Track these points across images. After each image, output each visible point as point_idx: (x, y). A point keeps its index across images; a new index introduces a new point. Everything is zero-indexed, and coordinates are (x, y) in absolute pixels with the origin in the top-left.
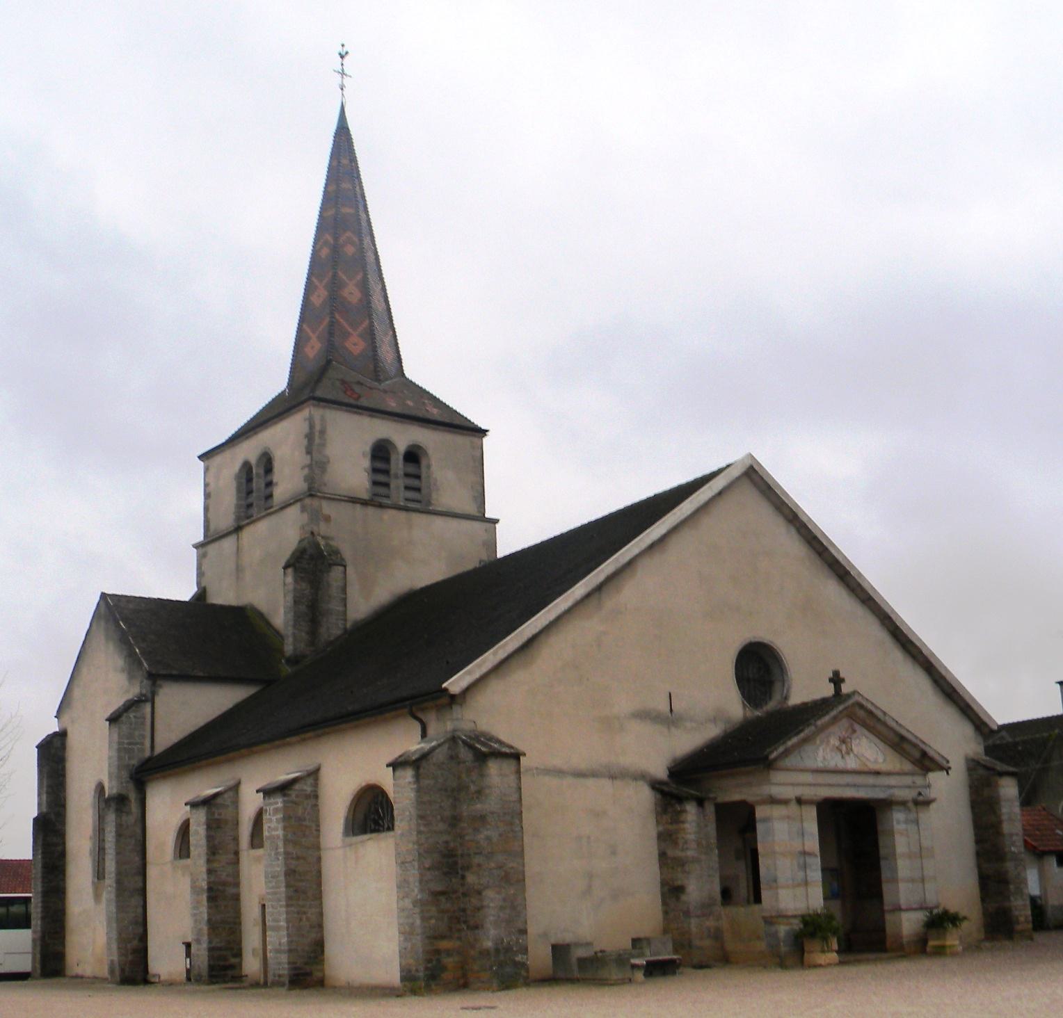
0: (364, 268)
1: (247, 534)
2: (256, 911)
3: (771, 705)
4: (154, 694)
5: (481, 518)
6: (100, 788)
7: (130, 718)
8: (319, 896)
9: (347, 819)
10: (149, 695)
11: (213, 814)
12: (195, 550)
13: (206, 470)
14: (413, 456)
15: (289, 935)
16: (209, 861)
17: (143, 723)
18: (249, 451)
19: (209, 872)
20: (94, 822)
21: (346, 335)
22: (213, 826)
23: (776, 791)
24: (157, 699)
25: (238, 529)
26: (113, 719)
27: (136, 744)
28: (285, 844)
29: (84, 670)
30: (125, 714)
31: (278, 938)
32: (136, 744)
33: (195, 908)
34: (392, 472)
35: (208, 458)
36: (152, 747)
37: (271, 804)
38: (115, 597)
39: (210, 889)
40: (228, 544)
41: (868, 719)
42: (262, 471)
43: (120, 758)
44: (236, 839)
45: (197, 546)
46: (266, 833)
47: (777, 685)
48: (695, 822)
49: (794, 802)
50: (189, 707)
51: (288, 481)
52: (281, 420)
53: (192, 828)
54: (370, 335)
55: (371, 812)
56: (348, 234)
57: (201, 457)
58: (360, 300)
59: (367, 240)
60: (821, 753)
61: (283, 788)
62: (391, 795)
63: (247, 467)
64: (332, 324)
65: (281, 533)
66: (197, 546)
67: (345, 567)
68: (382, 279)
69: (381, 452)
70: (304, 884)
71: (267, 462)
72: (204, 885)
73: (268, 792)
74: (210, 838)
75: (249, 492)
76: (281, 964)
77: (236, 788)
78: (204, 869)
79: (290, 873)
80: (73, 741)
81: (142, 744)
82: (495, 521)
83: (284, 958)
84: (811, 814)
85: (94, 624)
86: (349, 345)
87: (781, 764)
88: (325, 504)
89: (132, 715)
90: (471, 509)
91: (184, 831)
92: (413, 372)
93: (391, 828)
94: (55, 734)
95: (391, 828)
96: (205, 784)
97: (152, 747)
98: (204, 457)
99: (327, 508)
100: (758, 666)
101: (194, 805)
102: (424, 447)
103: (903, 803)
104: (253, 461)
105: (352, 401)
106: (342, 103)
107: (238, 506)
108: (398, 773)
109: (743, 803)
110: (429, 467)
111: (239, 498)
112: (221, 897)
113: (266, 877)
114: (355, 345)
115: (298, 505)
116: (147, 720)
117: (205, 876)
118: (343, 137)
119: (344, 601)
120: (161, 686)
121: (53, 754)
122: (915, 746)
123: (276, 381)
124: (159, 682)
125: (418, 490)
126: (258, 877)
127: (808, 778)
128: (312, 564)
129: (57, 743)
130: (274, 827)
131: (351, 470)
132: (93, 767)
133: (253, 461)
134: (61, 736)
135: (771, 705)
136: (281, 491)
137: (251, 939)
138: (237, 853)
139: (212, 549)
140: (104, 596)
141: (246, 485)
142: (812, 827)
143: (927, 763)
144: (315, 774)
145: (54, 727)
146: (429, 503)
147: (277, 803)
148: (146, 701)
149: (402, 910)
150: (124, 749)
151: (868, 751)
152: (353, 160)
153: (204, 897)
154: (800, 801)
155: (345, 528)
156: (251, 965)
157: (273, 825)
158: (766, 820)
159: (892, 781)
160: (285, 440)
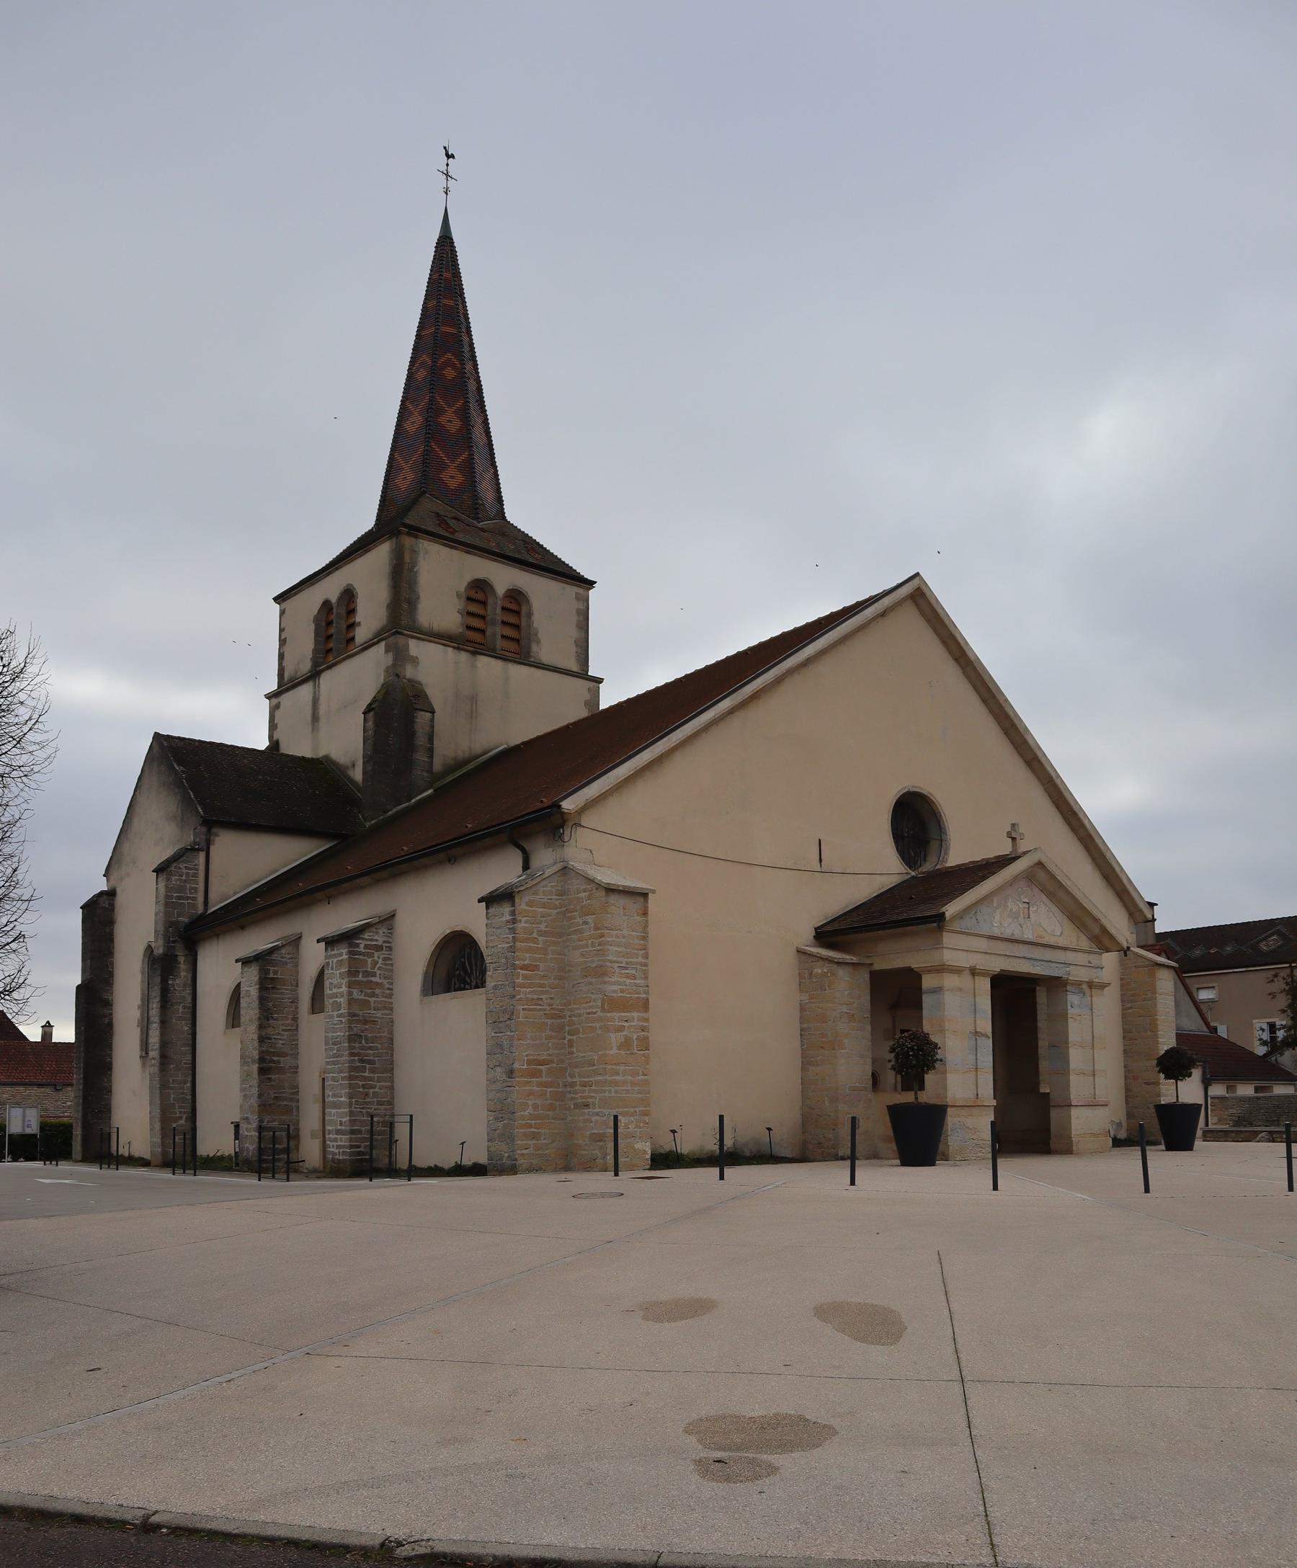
0: (464, 392)
1: (326, 679)
2: (316, 1088)
3: (927, 867)
5: (583, 674)
6: (149, 949)
8: (389, 1068)
9: (426, 974)
10: (203, 844)
11: (267, 972)
13: (282, 613)
14: (516, 597)
15: (351, 1113)
16: (261, 1027)
17: (195, 875)
18: (330, 589)
19: (262, 1040)
20: (245, 1078)
21: (443, 466)
22: (267, 985)
23: (949, 957)
24: (214, 850)
25: (314, 675)
26: (159, 870)
27: (188, 898)
28: (349, 1004)
29: (136, 821)
31: (339, 1117)
32: (188, 898)
33: (243, 1081)
36: (206, 903)
37: (335, 956)
38: (169, 738)
39: (262, 1060)
40: (305, 691)
41: (1044, 881)
42: (343, 612)
43: (167, 914)
44: (295, 1001)
45: (269, 696)
46: (327, 992)
47: (934, 845)
48: (847, 991)
49: (967, 972)
50: (244, 861)
51: (370, 615)
52: (367, 551)
53: (244, 988)
54: (468, 467)
55: (458, 965)
56: (449, 355)
57: (277, 599)
58: (460, 430)
59: (469, 366)
60: (997, 917)
61: (348, 937)
62: (482, 944)
63: (326, 605)
64: (427, 453)
65: (360, 677)
66: (269, 696)
67: (433, 712)
68: (483, 411)
69: (479, 590)
70: (370, 1051)
71: (349, 595)
72: (256, 1055)
73: (331, 942)
74: (262, 1000)
75: (329, 623)
76: (339, 1146)
77: (296, 941)
78: (255, 1037)
79: (353, 1038)
80: (120, 899)
81: (194, 899)
82: (600, 681)
83: (344, 1140)
84: (985, 985)
85: (146, 772)
86: (445, 476)
87: (956, 926)
90: (575, 667)
91: (236, 995)
92: (514, 515)
93: (481, 984)
94: (102, 894)
95: (481, 984)
96: (259, 940)
97: (206, 903)
98: (279, 599)
99: (415, 647)
100: (914, 821)
101: (246, 962)
102: (522, 598)
103: (1078, 984)
104: (334, 599)
105: (447, 534)
107: (315, 651)
108: (491, 910)
109: (909, 970)
110: (530, 615)
111: (317, 642)
112: (272, 1066)
113: (326, 1044)
114: (452, 477)
117: (256, 1044)
118: (445, 251)
121: (99, 917)
122: (1096, 920)
123: (366, 521)
125: (517, 627)
126: (317, 1043)
127: (982, 944)
128: (396, 712)
129: (104, 902)
130: (337, 986)
131: (440, 603)
132: (138, 930)
133: (334, 599)
134: (110, 894)
135: (927, 867)
136: (361, 635)
137: (310, 1120)
138: (295, 1019)
139: (286, 699)
140: (157, 737)
141: (324, 627)
142: (985, 1003)
143: (1106, 941)
144: (388, 920)
145: (102, 885)
146: (528, 654)
147: (341, 955)
149: (492, 1081)
150: (170, 904)
151: (1047, 922)
152: (457, 275)
153: (255, 1067)
154: (974, 972)
155: (434, 666)
156: (310, 1151)
157: (335, 981)
158: (938, 990)
159: (1070, 957)
160: (370, 579)
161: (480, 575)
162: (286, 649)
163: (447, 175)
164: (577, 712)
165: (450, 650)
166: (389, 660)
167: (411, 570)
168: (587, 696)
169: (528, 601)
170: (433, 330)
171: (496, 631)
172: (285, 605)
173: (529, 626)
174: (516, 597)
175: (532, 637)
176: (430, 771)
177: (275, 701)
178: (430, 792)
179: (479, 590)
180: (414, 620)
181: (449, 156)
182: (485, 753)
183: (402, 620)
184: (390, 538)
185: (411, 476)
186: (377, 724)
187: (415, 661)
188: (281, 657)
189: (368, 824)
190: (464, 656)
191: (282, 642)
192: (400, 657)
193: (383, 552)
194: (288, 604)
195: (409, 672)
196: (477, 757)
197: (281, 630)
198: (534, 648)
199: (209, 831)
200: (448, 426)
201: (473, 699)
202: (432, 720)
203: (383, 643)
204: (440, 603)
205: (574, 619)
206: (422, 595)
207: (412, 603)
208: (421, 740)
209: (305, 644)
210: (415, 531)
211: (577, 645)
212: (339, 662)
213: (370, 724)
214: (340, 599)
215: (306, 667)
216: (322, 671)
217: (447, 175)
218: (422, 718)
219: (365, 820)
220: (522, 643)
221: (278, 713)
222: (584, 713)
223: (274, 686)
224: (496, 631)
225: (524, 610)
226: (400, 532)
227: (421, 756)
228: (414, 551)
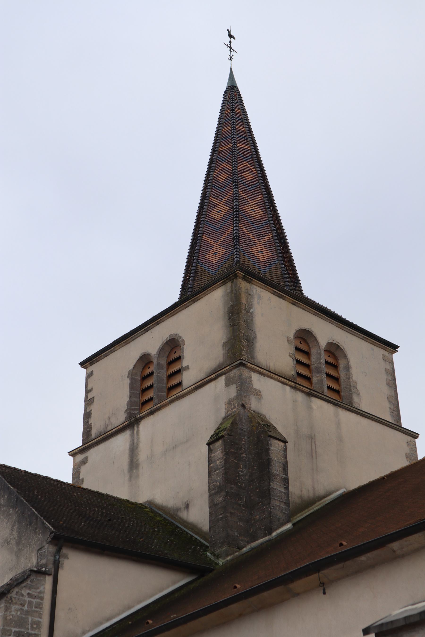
1: (146, 427)
4: (57, 565)
5: (396, 426)
7: (22, 595)
10: (51, 567)
12: (71, 458)
13: (89, 376)
17: (39, 606)
18: (151, 343)
25: (132, 422)
30: (16, 590)
34: (313, 367)
35: (91, 364)
40: (121, 442)
42: (164, 362)
45: (73, 454)
51: (198, 359)
52: (194, 301)
56: (246, 164)
57: (83, 364)
63: (145, 360)
71: (173, 345)
88: (255, 377)
89: (25, 592)
99: (258, 381)
106: (231, 70)
107: (130, 403)
110: (348, 368)
111: (132, 395)
114: (261, 252)
115: (222, 380)
116: (45, 601)
119: (286, 481)
120: (66, 557)
124: (64, 551)
131: (273, 345)
136: (188, 379)
139: (94, 454)
148: (45, 573)
155: (276, 402)
161: (306, 326)
162: (94, 408)
163: (230, 48)
164: (399, 463)
165: (288, 388)
166: (233, 391)
167: (247, 311)
168: (407, 450)
169: (345, 356)
170: (230, 146)
171: (320, 380)
172: (91, 369)
173: (349, 378)
174: (334, 351)
175: (351, 389)
176: (287, 504)
177: (80, 457)
178: (289, 526)
179: (304, 337)
180: (253, 357)
181: (231, 36)
182: (337, 490)
183: (238, 354)
184: (224, 283)
185: (221, 251)
186: (227, 453)
187: (258, 394)
188: (87, 415)
189: (221, 562)
190: (300, 396)
191: (89, 402)
192: (244, 388)
193: (215, 299)
194: (95, 367)
195: (254, 404)
196: (321, 498)
197: (87, 391)
198: (355, 399)
199: (59, 551)
200: (252, 213)
201: (312, 438)
202: (285, 450)
203: (223, 377)
204: (273, 345)
205: (384, 377)
206: (259, 335)
207: (250, 341)
208: (276, 469)
209: (118, 400)
210: (251, 276)
211: (390, 402)
212: (165, 405)
213: (218, 453)
214: (162, 350)
215: (121, 418)
216: (142, 418)
217: (230, 48)
218: (276, 446)
219: (218, 557)
220: (343, 394)
221: (84, 469)
222: (405, 463)
223: (78, 442)
224: (320, 380)
225: (342, 364)
226: (236, 276)
227: (277, 486)
228: (249, 295)
